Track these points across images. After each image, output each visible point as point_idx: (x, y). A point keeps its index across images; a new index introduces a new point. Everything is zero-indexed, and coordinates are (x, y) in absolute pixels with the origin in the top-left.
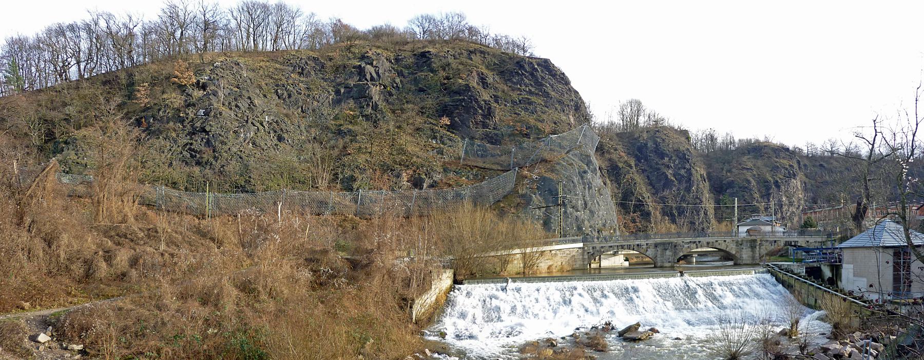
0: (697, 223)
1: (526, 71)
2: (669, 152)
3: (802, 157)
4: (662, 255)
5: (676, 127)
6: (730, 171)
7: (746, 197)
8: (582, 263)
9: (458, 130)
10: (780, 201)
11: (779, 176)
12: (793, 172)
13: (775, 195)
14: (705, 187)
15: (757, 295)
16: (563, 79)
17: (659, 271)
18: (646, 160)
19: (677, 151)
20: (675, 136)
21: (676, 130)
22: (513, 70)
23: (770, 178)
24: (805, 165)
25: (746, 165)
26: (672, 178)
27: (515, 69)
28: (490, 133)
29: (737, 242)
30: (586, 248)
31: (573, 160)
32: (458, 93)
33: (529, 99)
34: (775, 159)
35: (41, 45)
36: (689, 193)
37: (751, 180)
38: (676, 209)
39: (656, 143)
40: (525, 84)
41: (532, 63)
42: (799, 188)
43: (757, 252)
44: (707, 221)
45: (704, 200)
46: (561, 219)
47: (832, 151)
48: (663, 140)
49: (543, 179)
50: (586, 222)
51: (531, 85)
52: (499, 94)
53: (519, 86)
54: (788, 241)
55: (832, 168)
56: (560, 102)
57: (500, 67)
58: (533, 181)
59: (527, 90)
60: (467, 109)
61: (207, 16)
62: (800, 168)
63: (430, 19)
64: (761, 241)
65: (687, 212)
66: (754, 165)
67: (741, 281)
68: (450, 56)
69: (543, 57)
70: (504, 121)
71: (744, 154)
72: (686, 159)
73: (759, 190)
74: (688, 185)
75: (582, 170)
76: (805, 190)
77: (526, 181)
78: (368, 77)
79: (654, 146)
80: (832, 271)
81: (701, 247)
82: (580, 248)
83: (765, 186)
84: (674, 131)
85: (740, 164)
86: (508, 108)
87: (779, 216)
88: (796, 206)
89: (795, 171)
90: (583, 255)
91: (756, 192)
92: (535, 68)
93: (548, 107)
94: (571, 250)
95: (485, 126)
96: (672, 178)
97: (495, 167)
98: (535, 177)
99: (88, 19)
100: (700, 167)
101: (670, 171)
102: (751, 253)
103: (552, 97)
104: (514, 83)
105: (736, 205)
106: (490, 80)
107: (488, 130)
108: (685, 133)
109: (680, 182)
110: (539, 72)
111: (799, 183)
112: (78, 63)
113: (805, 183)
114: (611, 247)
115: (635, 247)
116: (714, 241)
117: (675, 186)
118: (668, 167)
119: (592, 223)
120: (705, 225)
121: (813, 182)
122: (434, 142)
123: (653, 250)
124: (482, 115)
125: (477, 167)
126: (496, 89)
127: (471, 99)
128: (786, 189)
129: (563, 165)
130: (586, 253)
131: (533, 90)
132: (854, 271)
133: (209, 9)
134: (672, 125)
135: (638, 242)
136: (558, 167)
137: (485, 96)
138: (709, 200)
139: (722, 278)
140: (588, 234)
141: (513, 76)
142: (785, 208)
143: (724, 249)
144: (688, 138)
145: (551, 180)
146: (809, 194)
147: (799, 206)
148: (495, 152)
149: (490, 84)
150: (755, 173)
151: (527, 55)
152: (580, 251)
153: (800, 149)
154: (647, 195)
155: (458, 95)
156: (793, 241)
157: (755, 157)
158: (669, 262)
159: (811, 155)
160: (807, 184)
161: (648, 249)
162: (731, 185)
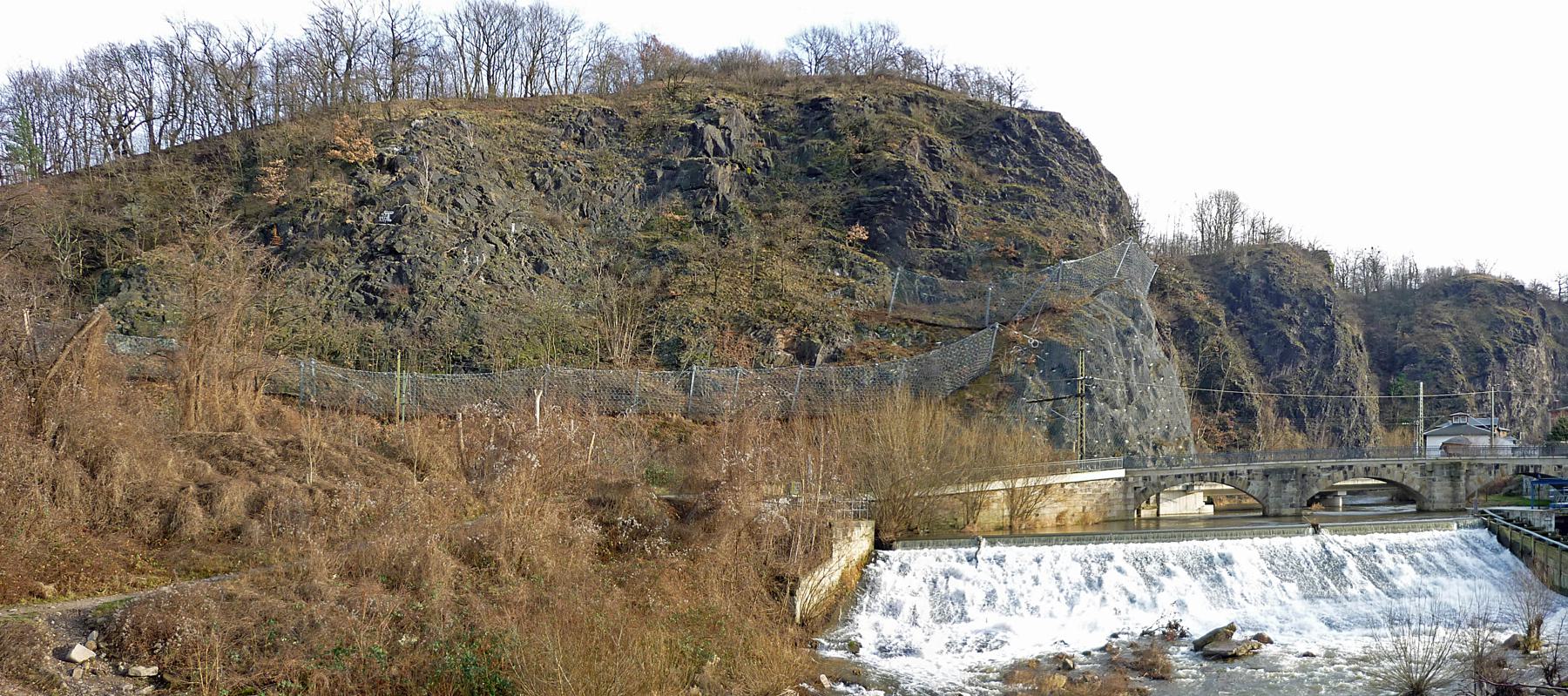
0: (1346, 431)
3: (1548, 302)
4: (1279, 493)
6: (1409, 330)
8: (1123, 508)
12: (1532, 332)
13: (1497, 377)
15: (1463, 571)
16: (1087, 153)
17: (1271, 524)
18: (1247, 308)
20: (1304, 262)
23: (1487, 344)
24: (1555, 319)
25: (1441, 319)
26: (1298, 344)
27: (992, 133)
29: (1423, 467)
30: (1131, 480)
32: (883, 178)
33: (1020, 191)
34: (1497, 307)
35: (77, 86)
39: (1265, 275)
40: (1012, 162)
41: (1026, 121)
43: (1463, 487)
49: (1048, 345)
50: (1131, 429)
51: (1025, 163)
52: (963, 180)
53: (1001, 166)
56: (1080, 196)
57: (965, 128)
58: (1029, 350)
59: (1018, 173)
61: (398, 29)
63: (828, 36)
64: (1469, 465)
66: (1456, 319)
67: (1430, 543)
69: (1049, 107)
71: (1436, 297)
73: (1465, 368)
77: (1014, 350)
78: (710, 147)
81: (1354, 476)
82: (1119, 479)
83: (1477, 359)
85: (1429, 317)
86: (980, 209)
90: (1125, 493)
92: (1032, 131)
93: (1057, 207)
94: (1102, 482)
95: (935, 242)
96: (1298, 344)
97: (955, 322)
99: (168, 35)
101: (1294, 330)
102: (1450, 489)
106: (945, 154)
107: (941, 250)
109: (1312, 351)
111: (1543, 353)
112: (149, 120)
114: (1180, 476)
117: (1303, 358)
118: (1290, 322)
119: (1143, 430)
123: (1261, 483)
126: (956, 171)
127: (909, 191)
131: (1028, 172)
133: (401, 16)
136: (1076, 322)
139: (1394, 538)
141: (990, 147)
147: (1543, 398)
149: (945, 162)
150: (1457, 333)
151: (1018, 105)
152: (1120, 485)
157: (1459, 304)
158: (1292, 506)
161: (1252, 482)
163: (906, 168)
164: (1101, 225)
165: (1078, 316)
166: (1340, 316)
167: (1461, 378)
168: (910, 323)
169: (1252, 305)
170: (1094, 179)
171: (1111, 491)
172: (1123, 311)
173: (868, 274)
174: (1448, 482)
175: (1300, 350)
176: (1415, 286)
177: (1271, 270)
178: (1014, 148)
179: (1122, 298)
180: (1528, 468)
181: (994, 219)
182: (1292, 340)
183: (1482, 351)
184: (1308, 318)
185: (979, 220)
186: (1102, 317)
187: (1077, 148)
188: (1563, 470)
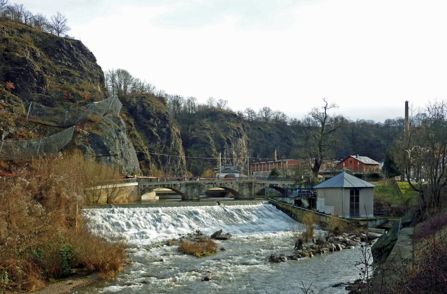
0: (176, 170)
1: (64, 49)
2: (154, 114)
3: (245, 121)
4: (192, 192)
6: (193, 130)
7: (207, 151)
9: (19, 94)
11: (230, 136)
12: (240, 133)
13: (228, 150)
14: (180, 142)
15: (270, 217)
16: (92, 58)
17: (190, 202)
19: (159, 114)
20: (157, 102)
22: (54, 48)
23: (224, 137)
24: (248, 128)
25: (206, 126)
26: (157, 135)
27: (56, 47)
28: (44, 97)
29: (240, 184)
30: (139, 186)
31: (110, 121)
32: (18, 64)
33: (68, 72)
34: (227, 122)
37: (210, 138)
38: (160, 158)
39: (143, 106)
40: (64, 60)
41: (68, 43)
43: (253, 191)
44: (183, 168)
47: (266, 118)
49: (92, 135)
50: (124, 168)
51: (69, 60)
52: (46, 66)
53: (60, 61)
55: (267, 131)
56: (91, 75)
57: (44, 44)
58: (85, 136)
59: (67, 64)
60: (25, 78)
62: (244, 130)
64: (255, 183)
66: (211, 126)
67: (257, 208)
68: (5, 32)
70: (52, 88)
71: (203, 117)
72: (166, 120)
73: (216, 146)
75: (117, 129)
76: (248, 147)
77: (79, 136)
79: (142, 109)
80: (309, 202)
81: (216, 187)
82: (136, 186)
83: (220, 143)
84: (156, 98)
85: (201, 125)
86: (54, 78)
89: (241, 132)
90: (138, 191)
91: (214, 147)
92: (71, 48)
93: (83, 79)
94: (131, 187)
95: (39, 91)
96: (157, 135)
97: (52, 124)
98: (86, 133)
101: (155, 129)
102: (249, 191)
103: (85, 71)
104: (56, 58)
106: (39, 55)
107: (41, 94)
108: (299, 122)
109: (162, 138)
110: (74, 51)
111: (244, 142)
113: (248, 142)
114: (156, 185)
116: (225, 183)
117: (159, 140)
118: (153, 126)
119: (127, 168)
121: (253, 141)
122: (3, 102)
123: (185, 188)
124: (36, 83)
125: (39, 123)
126: (43, 62)
127: (28, 70)
129: (104, 125)
130: (139, 190)
131: (71, 64)
132: (325, 202)
136: (101, 126)
137: (37, 68)
139: (246, 206)
141: (55, 53)
143: (231, 188)
145: (98, 136)
146: (251, 150)
147: (244, 159)
148: (50, 112)
149: (39, 58)
150: (212, 132)
152: (136, 188)
155: (17, 66)
157: (212, 121)
161: (182, 188)
163: (26, 60)
164: (99, 87)
165: (101, 124)
166: (172, 124)
167: (214, 150)
168: (36, 124)
169: (138, 118)
170: (95, 68)
171: (134, 190)
172: (115, 122)
173: (16, 103)
174: (248, 189)
175: (156, 137)
176: (194, 112)
177: (145, 105)
178: (64, 54)
179: (114, 117)
180: (273, 185)
181: (60, 83)
182: (154, 133)
183: (222, 140)
184: (160, 124)
185: (54, 83)
186: (109, 124)
187: (88, 55)
188: (285, 186)
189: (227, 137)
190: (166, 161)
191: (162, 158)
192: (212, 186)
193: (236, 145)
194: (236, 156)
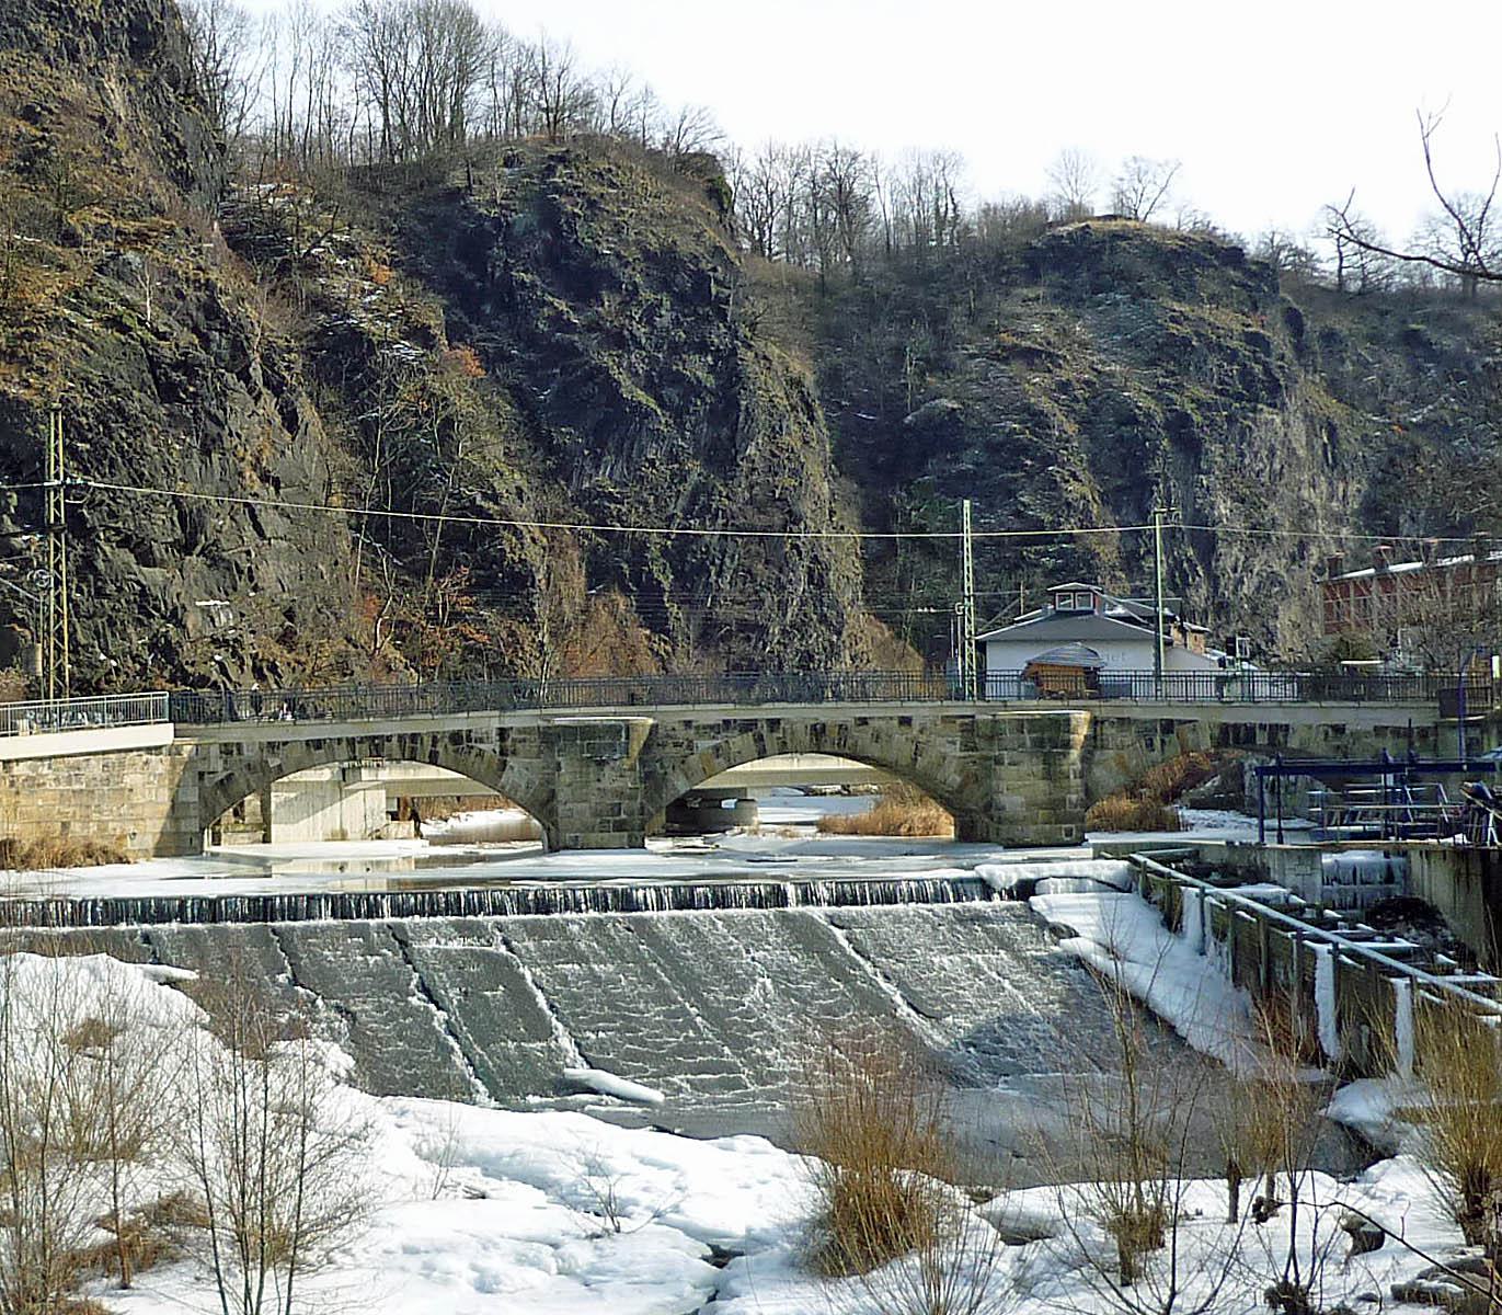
5: (657, 140)
10: (1200, 517)
12: (1267, 371)
13: (1177, 492)
19: (664, 264)
21: (653, 153)
24: (1329, 337)
26: (642, 396)
36: (728, 478)
42: (1301, 453)
44: (823, 619)
45: (806, 507)
46: (58, 597)
48: (592, 204)
54: (1235, 726)
62: (1300, 350)
65: (719, 574)
74: (725, 431)
81: (783, 750)
82: (157, 749)
87: (1199, 596)
88: (1290, 547)
89: (1274, 363)
96: (642, 396)
100: (784, 343)
105: (968, 535)
111: (1299, 430)
113: (1332, 431)
114: (318, 744)
115: (440, 749)
117: (657, 436)
120: (816, 639)
128: (1233, 458)
134: (634, 125)
135: (460, 722)
138: (832, 513)
140: (203, 681)
142: (1230, 556)
144: (718, 194)
147: (1302, 546)
153: (1298, 253)
154: (509, 481)
156: (1263, 727)
159: (1354, 286)
160: (1341, 434)
162: (944, 434)
183: (1134, 421)
188: (1345, 740)
189: (1172, 402)
190: (702, 569)
191: (680, 553)
192: (739, 742)
193: (1242, 455)
194: (1239, 526)
